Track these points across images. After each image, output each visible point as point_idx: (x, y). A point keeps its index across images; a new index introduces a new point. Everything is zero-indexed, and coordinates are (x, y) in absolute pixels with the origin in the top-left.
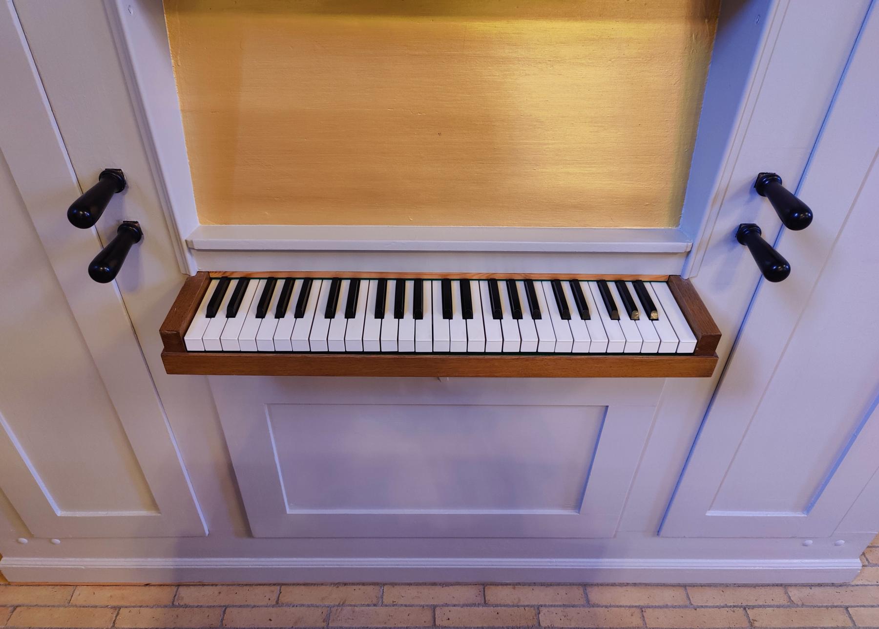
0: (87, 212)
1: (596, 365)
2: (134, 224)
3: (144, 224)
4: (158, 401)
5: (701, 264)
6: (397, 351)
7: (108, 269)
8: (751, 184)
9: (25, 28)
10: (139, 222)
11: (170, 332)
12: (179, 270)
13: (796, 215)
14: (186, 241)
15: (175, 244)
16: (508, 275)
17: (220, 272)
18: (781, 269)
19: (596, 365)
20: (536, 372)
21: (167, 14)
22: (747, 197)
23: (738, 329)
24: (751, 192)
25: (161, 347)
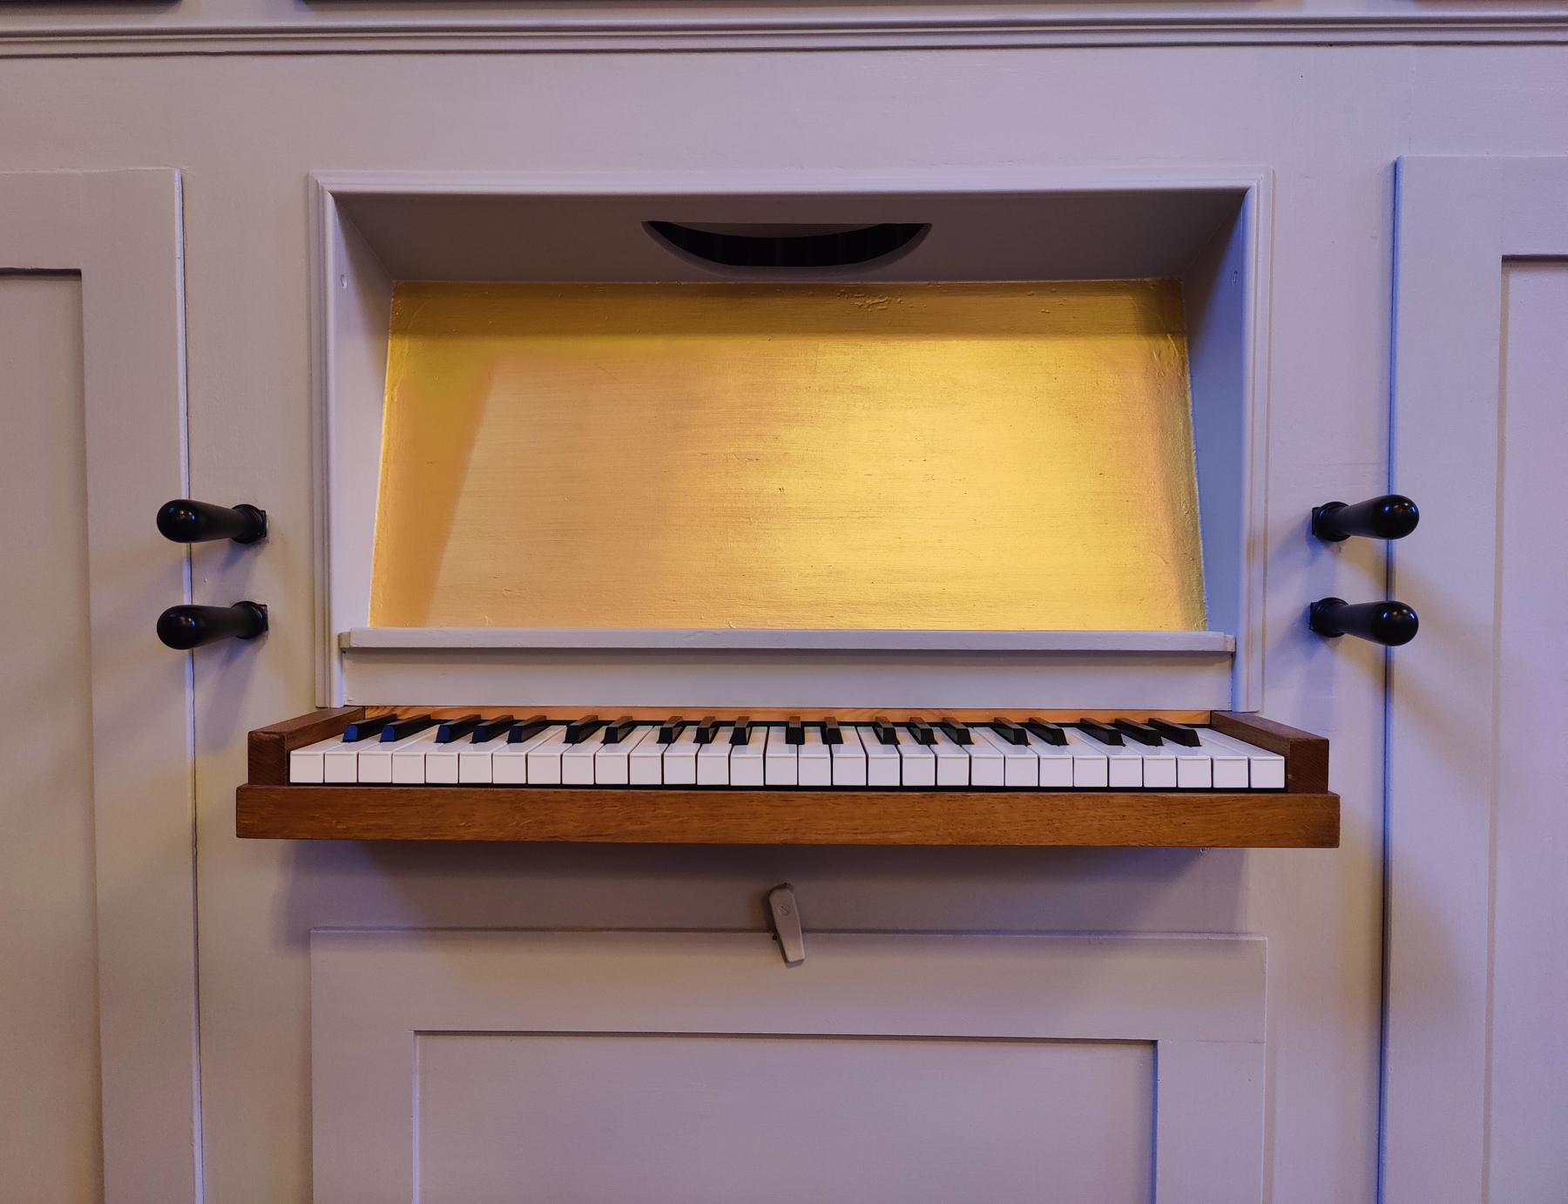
0: (193, 514)
1: (1093, 813)
2: (262, 609)
3: (275, 613)
4: (194, 1044)
5: (1263, 687)
6: (694, 783)
7: (193, 623)
8: (1306, 527)
9: (190, 373)
10: (268, 607)
11: (267, 735)
12: (314, 697)
13: (1387, 509)
14: (339, 636)
15: (318, 560)
16: (908, 712)
17: (385, 707)
18: (1399, 617)
19: (1093, 813)
20: (973, 831)
21: (392, 340)
22: (1304, 551)
23: (1380, 836)
24: (1310, 542)
25: (242, 778)
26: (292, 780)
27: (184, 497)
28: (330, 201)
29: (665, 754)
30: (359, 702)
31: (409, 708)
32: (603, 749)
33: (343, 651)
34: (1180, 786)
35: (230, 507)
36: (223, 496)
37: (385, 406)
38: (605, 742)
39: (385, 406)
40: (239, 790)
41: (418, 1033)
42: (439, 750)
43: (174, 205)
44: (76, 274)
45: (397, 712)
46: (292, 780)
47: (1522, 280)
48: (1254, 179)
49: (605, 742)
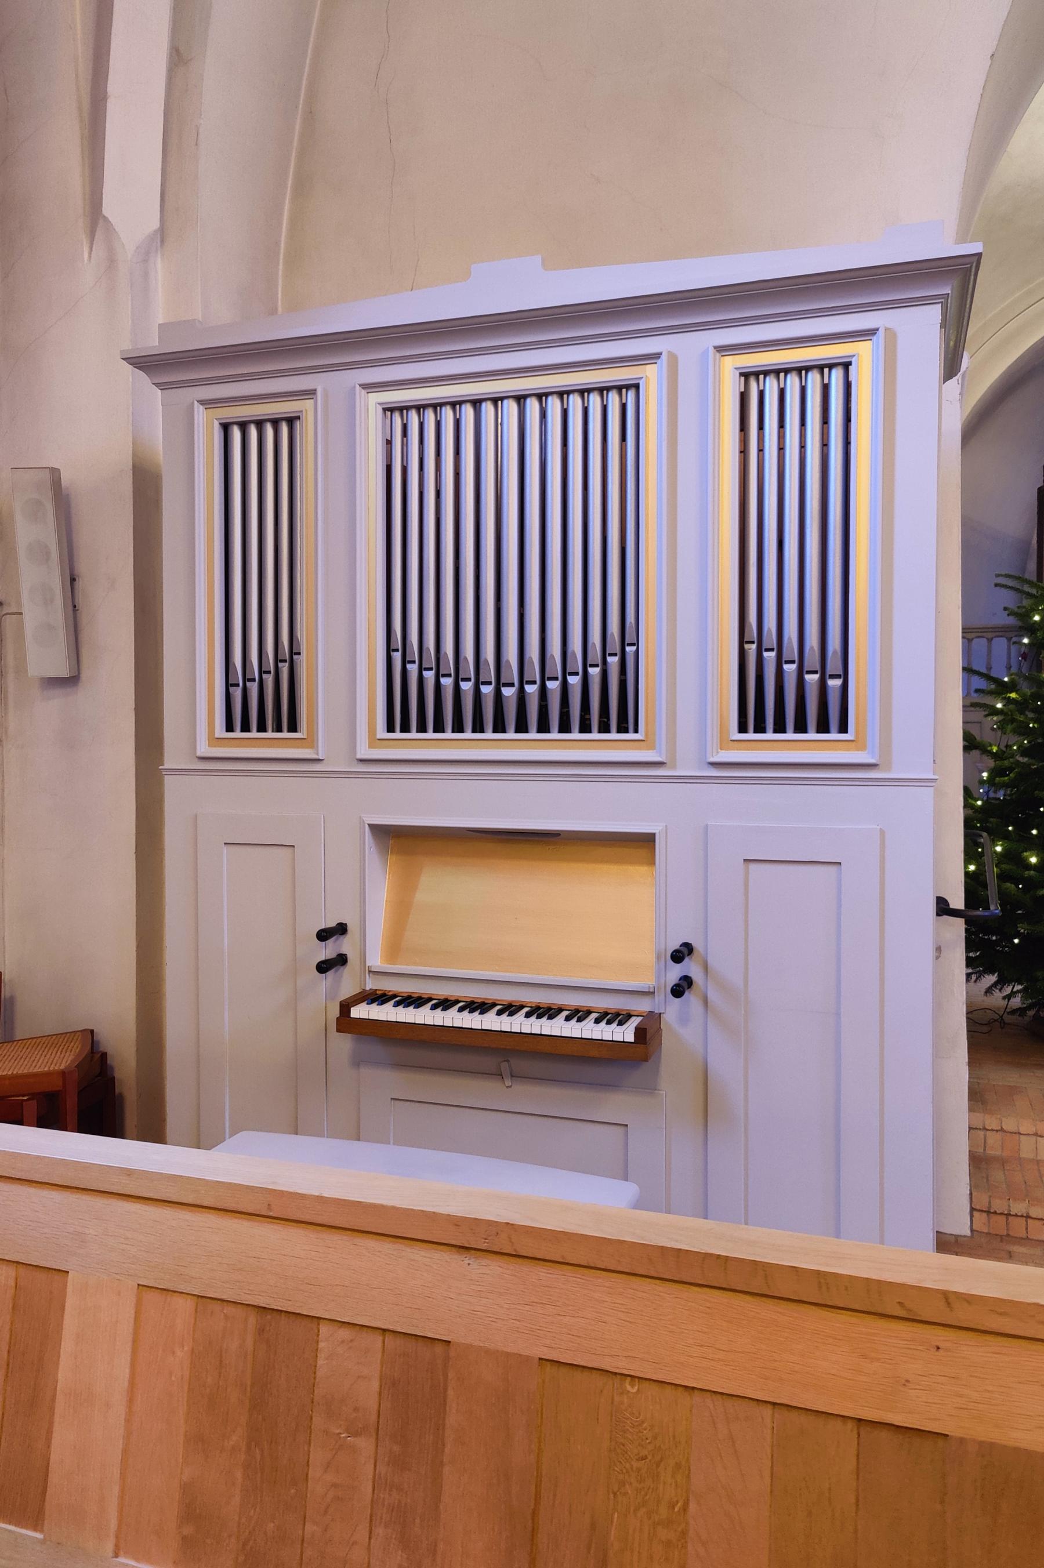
3: (350, 957)
26: (351, 1016)
27: (323, 927)
28: (367, 826)
29: (625, 1032)
30: (375, 988)
31: (390, 991)
32: (536, 1022)
33: (370, 972)
34: (614, 1040)
35: (335, 925)
36: (332, 923)
37: (387, 880)
38: (577, 1021)
39: (387, 880)
40: (337, 1018)
41: (225, 843)
42: (406, 1010)
43: (317, 688)
44: (294, 846)
45: (386, 992)
46: (351, 1016)
47: (753, 867)
48: (657, 829)
49: (577, 1021)
